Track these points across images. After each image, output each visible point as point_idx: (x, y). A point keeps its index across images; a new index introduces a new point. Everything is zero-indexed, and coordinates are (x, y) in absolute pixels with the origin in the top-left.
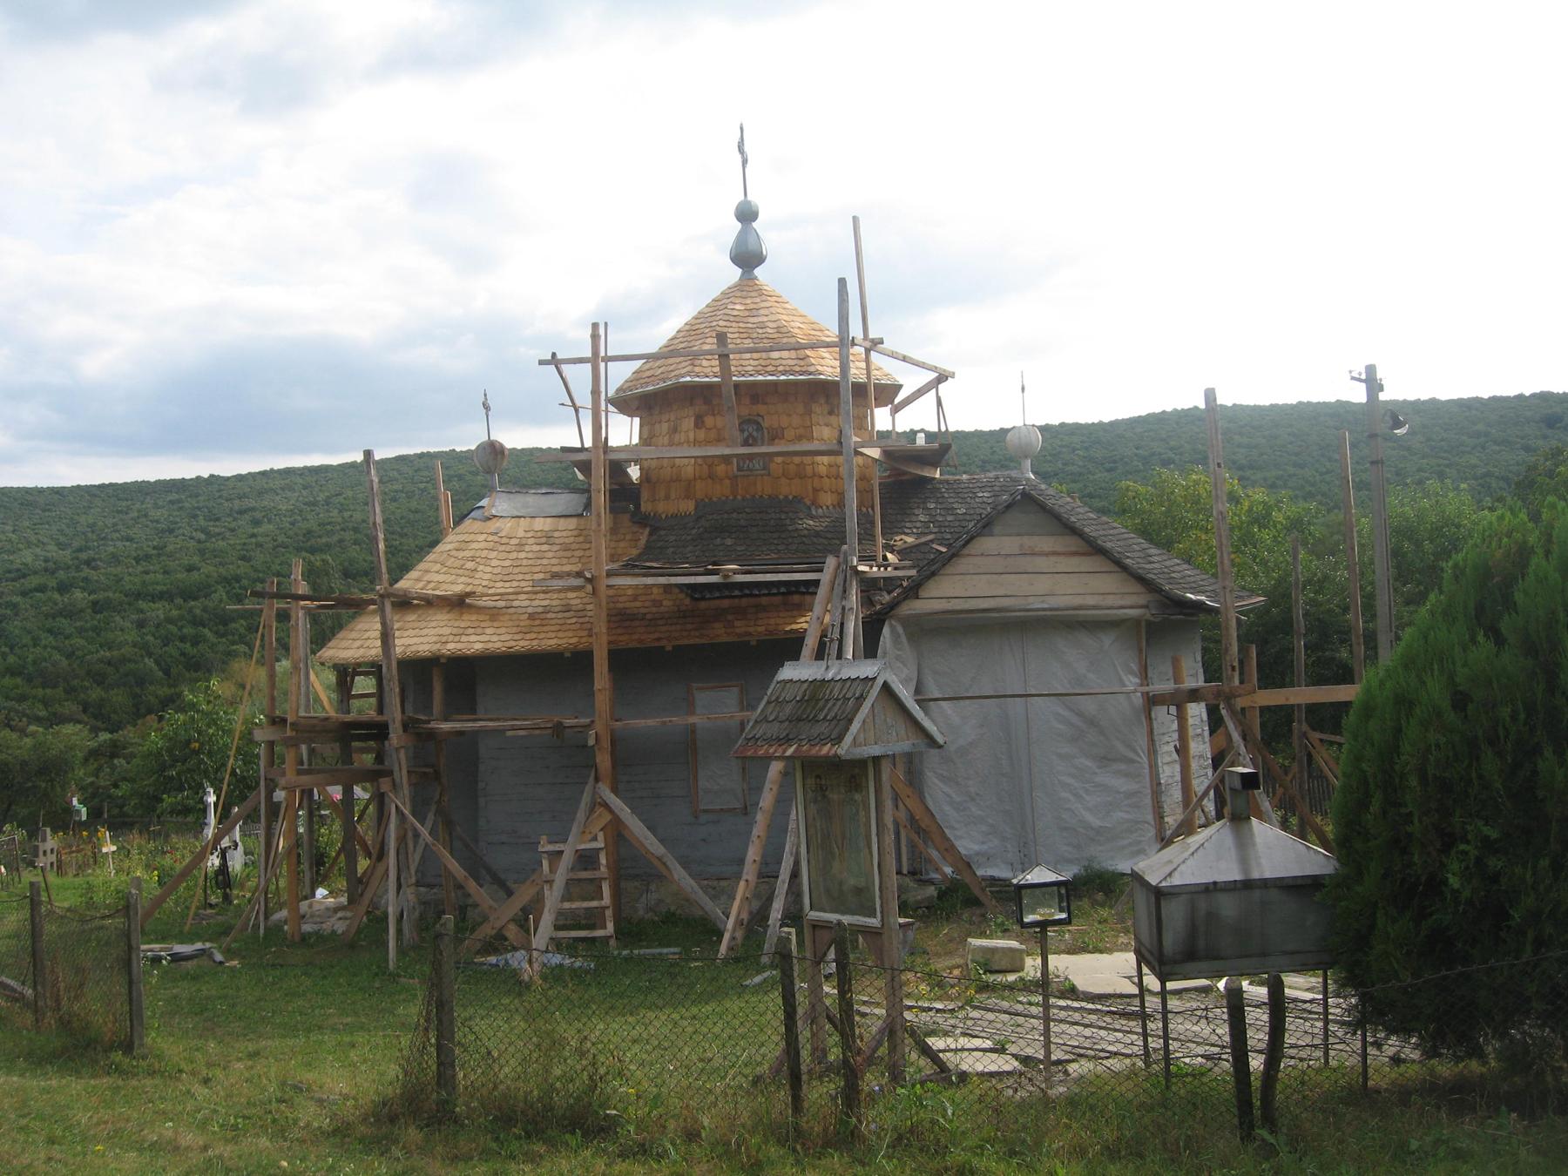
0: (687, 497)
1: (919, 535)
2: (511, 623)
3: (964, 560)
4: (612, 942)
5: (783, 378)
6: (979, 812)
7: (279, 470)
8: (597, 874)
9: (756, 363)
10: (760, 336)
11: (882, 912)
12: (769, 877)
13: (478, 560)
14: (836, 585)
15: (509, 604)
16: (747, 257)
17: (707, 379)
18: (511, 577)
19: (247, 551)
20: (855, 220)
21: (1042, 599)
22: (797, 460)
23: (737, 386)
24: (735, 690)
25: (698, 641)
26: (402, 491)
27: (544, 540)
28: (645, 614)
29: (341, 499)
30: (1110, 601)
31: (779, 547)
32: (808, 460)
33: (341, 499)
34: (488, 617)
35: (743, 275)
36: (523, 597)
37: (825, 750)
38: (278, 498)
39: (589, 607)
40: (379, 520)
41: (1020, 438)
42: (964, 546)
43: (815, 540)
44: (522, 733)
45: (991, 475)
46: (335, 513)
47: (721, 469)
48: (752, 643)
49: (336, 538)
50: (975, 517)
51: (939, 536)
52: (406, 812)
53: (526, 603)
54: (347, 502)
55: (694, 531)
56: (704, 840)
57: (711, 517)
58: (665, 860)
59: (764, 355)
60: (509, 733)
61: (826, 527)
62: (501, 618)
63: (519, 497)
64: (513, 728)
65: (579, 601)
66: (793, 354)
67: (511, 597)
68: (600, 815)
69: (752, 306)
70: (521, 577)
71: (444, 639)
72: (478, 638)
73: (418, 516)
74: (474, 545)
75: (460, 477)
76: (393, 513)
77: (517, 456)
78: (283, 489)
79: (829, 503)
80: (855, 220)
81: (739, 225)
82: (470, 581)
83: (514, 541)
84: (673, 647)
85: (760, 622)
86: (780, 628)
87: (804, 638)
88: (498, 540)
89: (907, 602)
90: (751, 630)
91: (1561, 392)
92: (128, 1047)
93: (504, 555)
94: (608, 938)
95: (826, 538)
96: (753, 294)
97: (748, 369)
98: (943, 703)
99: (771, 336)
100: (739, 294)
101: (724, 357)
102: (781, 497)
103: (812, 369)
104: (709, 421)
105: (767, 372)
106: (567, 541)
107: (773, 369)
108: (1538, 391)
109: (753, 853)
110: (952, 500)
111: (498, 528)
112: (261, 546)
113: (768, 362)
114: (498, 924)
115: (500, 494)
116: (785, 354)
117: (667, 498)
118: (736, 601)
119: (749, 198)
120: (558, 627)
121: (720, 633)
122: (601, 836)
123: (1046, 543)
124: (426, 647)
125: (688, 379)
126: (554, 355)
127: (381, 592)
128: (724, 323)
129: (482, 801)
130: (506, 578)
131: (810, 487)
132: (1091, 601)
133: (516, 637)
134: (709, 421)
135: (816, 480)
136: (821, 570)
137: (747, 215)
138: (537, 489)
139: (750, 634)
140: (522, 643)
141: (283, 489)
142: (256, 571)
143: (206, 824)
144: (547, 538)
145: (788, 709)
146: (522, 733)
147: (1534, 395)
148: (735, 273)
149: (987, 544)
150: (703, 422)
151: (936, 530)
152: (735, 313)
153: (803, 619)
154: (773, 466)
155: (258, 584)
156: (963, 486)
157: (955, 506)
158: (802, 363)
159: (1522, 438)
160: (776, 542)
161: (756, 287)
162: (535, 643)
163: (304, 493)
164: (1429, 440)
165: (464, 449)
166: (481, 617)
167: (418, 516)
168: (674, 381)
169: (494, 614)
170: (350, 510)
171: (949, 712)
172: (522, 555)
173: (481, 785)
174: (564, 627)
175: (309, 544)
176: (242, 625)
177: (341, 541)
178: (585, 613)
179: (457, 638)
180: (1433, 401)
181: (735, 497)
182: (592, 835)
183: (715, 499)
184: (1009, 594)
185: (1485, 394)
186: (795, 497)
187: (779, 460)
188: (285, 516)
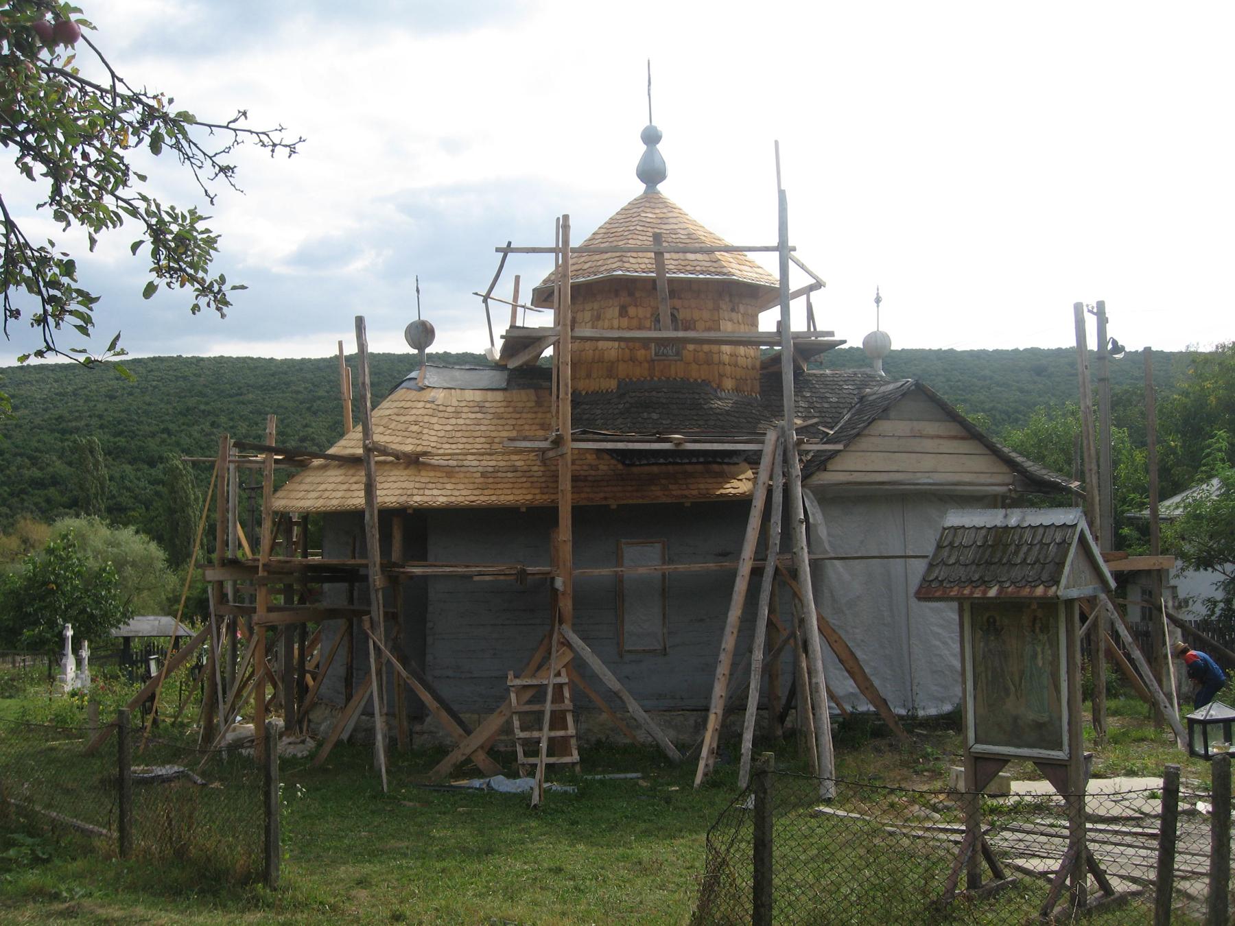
0: (610, 377)
1: (805, 418)
2: (466, 481)
3: (864, 439)
4: (578, 768)
5: (701, 276)
6: (864, 657)
7: (35, 366)
8: (563, 707)
9: (676, 263)
10: (674, 240)
11: (1070, 746)
12: (683, 710)
13: (421, 424)
14: (777, 456)
15: (460, 463)
16: (651, 173)
17: (636, 274)
18: (455, 440)
19: (8, 430)
20: (776, 143)
21: (927, 475)
22: (706, 348)
23: (671, 281)
24: (658, 546)
25: (640, 501)
26: (137, 387)
27: (477, 409)
28: (586, 476)
29: (86, 391)
30: (983, 479)
31: (700, 423)
32: (715, 348)
33: (86, 391)
34: (444, 474)
35: (645, 192)
36: (470, 457)
37: (1040, 591)
38: (33, 388)
39: (535, 468)
40: (367, 381)
41: (876, 341)
42: (865, 428)
43: (727, 417)
44: (487, 578)
45: (851, 371)
46: (81, 402)
47: (641, 354)
48: (686, 505)
49: (83, 423)
50: (847, 405)
51: (822, 420)
52: (382, 647)
53: (475, 463)
54: (92, 394)
55: (621, 406)
56: (627, 677)
57: (634, 394)
58: (621, 694)
59: (681, 256)
60: (476, 578)
61: (732, 407)
62: (457, 476)
63: (446, 372)
64: (480, 574)
65: (523, 463)
66: (706, 257)
67: (460, 457)
68: (563, 653)
69: (662, 216)
70: (464, 440)
71: (409, 492)
72: (440, 492)
73: (152, 408)
74: (414, 411)
75: (185, 378)
76: (130, 404)
77: (232, 362)
78: (37, 381)
79: (729, 388)
80: (776, 143)
81: (644, 148)
82: (418, 442)
83: (449, 409)
84: (618, 505)
85: (691, 487)
86: (711, 492)
87: (752, 500)
88: (435, 407)
89: (818, 473)
90: (686, 492)
91: (1046, 349)
92: (265, 876)
93: (444, 421)
94: (574, 764)
95: (735, 416)
96: (660, 206)
97: (675, 267)
98: (836, 562)
99: (683, 241)
100: (648, 205)
101: (659, 254)
102: (692, 380)
103: (725, 270)
104: (632, 311)
105: (687, 271)
106: (498, 410)
107: (693, 268)
108: (1029, 347)
109: (719, 690)
110: (823, 391)
111: (434, 397)
112: (21, 427)
113: (687, 262)
114: (468, 751)
115: (428, 368)
116: (699, 256)
117: (589, 376)
118: (663, 467)
119: (653, 124)
120: (511, 486)
121: (657, 495)
122: (563, 672)
123: (931, 428)
124: (393, 499)
125: (620, 273)
126: (498, 250)
127: (370, 446)
128: (641, 228)
129: (430, 640)
130: (451, 441)
131: (716, 373)
132: (967, 478)
133: (476, 492)
134: (632, 311)
135: (721, 366)
136: (763, 442)
137: (651, 137)
138: (461, 365)
139: (686, 496)
140: (482, 498)
141: (37, 381)
142: (17, 447)
143: (64, 655)
144: (480, 407)
145: (970, 555)
146: (487, 578)
147: (1026, 350)
148: (640, 188)
149: (885, 426)
150: (627, 312)
151: (818, 415)
152: (649, 220)
153: (728, 486)
154: (685, 352)
155: (19, 458)
156: (828, 379)
157: (828, 395)
158: (715, 265)
159: (1018, 382)
160: (695, 418)
161: (661, 200)
162: (493, 498)
163: (56, 385)
164: (948, 380)
165: (190, 356)
166: (439, 474)
167: (152, 408)
168: (605, 274)
169: (449, 472)
170: (94, 401)
171: (841, 570)
172: (461, 421)
173: (429, 625)
174: (516, 485)
175: (61, 426)
176: (5, 491)
177: (87, 425)
178: (532, 473)
179: (421, 492)
180: (951, 351)
181: (652, 378)
182: (556, 671)
183: (635, 380)
184: (901, 470)
185: (990, 347)
186: (703, 380)
187: (691, 347)
188: (38, 403)
